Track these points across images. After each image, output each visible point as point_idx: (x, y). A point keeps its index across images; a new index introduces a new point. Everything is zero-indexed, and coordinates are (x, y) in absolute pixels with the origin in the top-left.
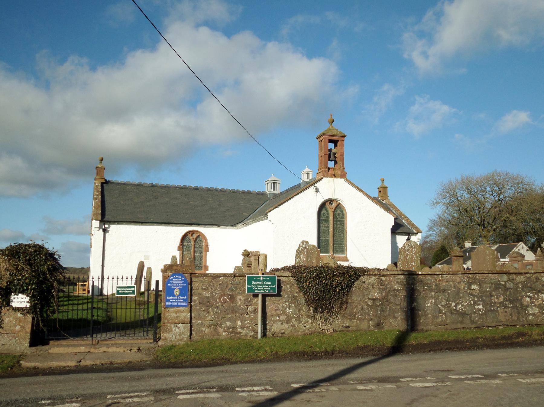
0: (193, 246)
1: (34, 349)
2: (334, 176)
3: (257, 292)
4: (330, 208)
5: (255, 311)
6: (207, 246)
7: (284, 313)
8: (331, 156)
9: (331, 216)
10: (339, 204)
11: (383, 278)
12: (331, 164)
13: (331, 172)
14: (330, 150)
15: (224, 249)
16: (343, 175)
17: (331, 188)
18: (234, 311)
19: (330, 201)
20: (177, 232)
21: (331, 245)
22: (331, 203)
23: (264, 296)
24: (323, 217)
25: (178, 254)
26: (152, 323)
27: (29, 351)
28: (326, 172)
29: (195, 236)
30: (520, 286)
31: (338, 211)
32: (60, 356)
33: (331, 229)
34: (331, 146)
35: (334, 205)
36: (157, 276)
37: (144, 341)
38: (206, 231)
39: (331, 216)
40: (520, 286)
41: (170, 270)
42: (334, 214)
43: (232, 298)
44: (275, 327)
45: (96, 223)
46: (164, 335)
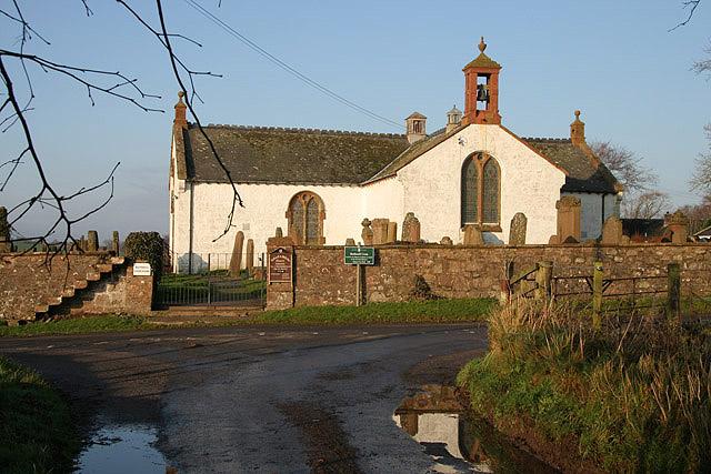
0: (305, 213)
1: (155, 313)
2: (485, 121)
3: (355, 263)
4: (478, 164)
5: (354, 281)
6: (323, 211)
7: (382, 283)
8: (481, 94)
9: (479, 180)
10: (491, 158)
11: (482, 251)
12: (481, 106)
13: (481, 116)
14: (480, 87)
15: (348, 212)
16: (497, 120)
17: (478, 137)
18: (334, 280)
19: (479, 155)
20: (282, 194)
21: (479, 211)
22: (479, 158)
23: (363, 266)
24: (469, 176)
25: (284, 224)
26: (258, 296)
27: (151, 314)
28: (474, 117)
29: (307, 199)
30: (631, 259)
31: (489, 167)
32: (178, 318)
33: (479, 196)
34: (482, 80)
35: (484, 159)
36: (261, 249)
37: (252, 310)
38: (318, 190)
39: (479, 180)
40: (631, 259)
41: (276, 245)
42: (484, 170)
43: (332, 269)
44: (375, 297)
45: (178, 183)
46: (269, 303)
